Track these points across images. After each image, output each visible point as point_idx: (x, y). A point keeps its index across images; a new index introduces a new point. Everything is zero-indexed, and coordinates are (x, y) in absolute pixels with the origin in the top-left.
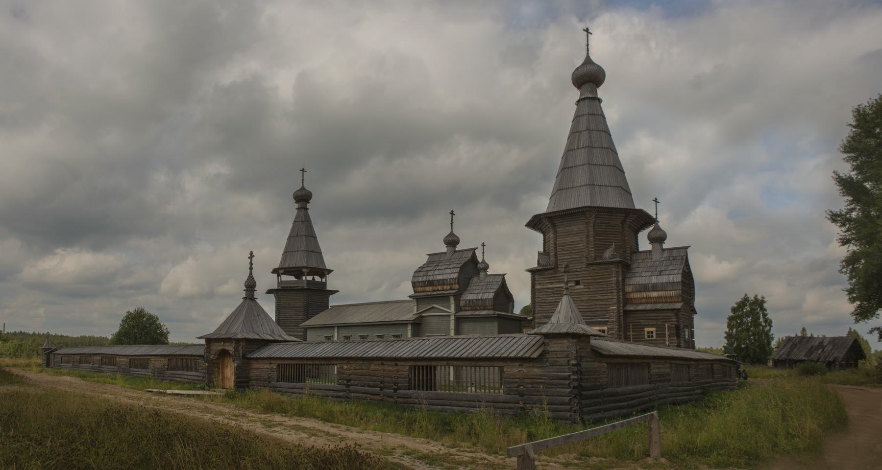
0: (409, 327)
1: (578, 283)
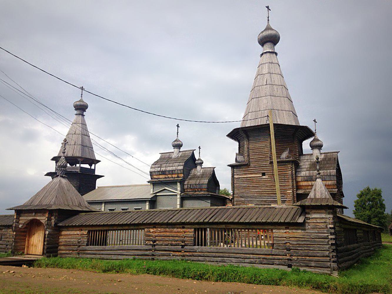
0: (148, 203)
1: (264, 174)
